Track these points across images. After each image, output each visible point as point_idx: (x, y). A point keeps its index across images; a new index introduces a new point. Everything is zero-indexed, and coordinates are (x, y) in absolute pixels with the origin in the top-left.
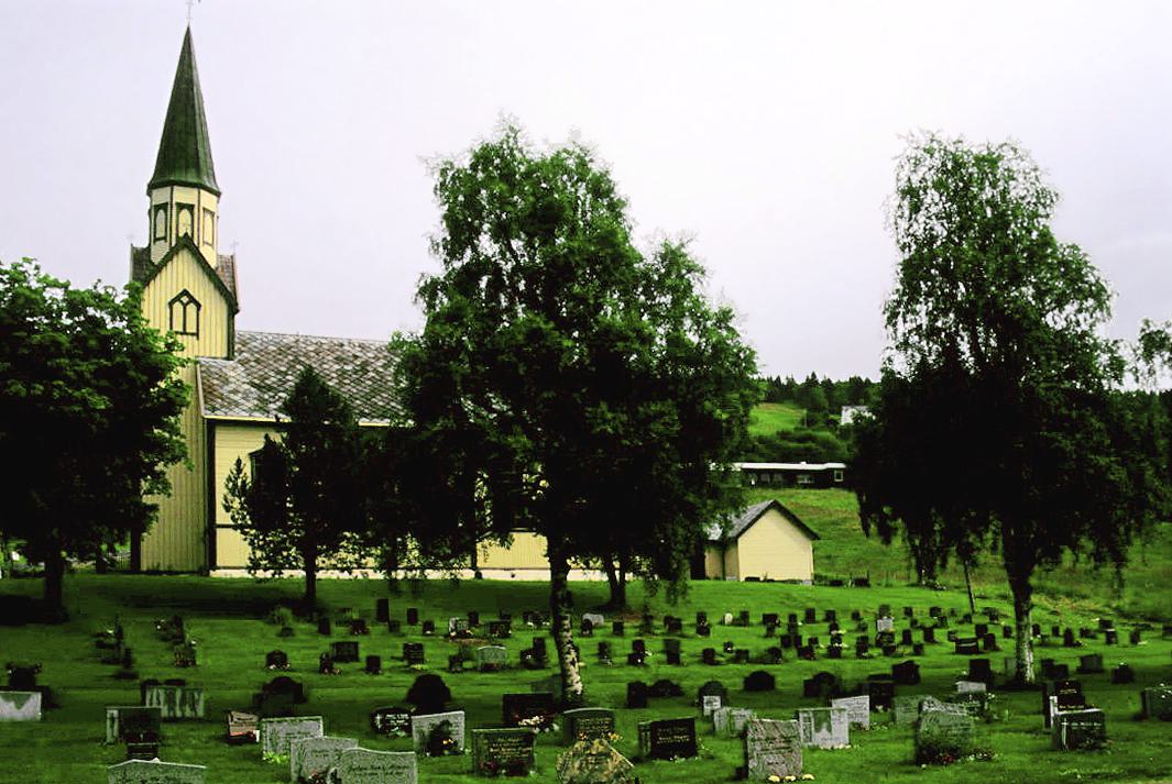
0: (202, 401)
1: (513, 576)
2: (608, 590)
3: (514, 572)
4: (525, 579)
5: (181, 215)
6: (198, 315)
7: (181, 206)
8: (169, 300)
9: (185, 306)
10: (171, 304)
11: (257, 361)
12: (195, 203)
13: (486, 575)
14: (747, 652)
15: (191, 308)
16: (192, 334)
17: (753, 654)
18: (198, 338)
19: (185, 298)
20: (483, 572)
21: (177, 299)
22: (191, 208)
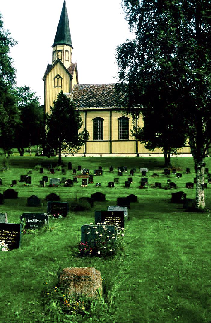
0: (91, 108)
1: (150, 156)
2: (164, 161)
3: (150, 154)
4: (161, 157)
5: (59, 53)
6: (62, 81)
7: (59, 51)
8: (54, 78)
9: (58, 79)
10: (54, 79)
11: (78, 93)
12: (62, 49)
13: (141, 155)
14: (160, 184)
15: (60, 80)
16: (60, 87)
17: (163, 185)
18: (61, 88)
19: (58, 77)
20: (140, 154)
21: (56, 77)
22: (61, 51)
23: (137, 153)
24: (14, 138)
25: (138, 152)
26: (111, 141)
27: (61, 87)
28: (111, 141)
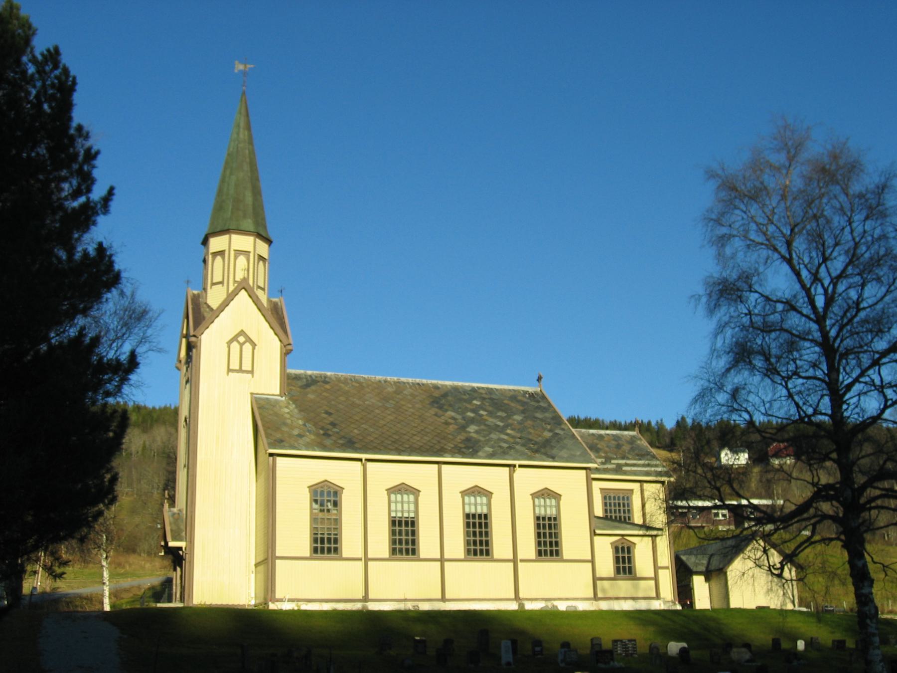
9: (241, 345)
10: (230, 343)
15: (248, 347)
21: (235, 339)
23: (517, 598)
24: (49, 163)
25: (521, 595)
26: (442, 560)
27: (252, 372)
28: (442, 560)
